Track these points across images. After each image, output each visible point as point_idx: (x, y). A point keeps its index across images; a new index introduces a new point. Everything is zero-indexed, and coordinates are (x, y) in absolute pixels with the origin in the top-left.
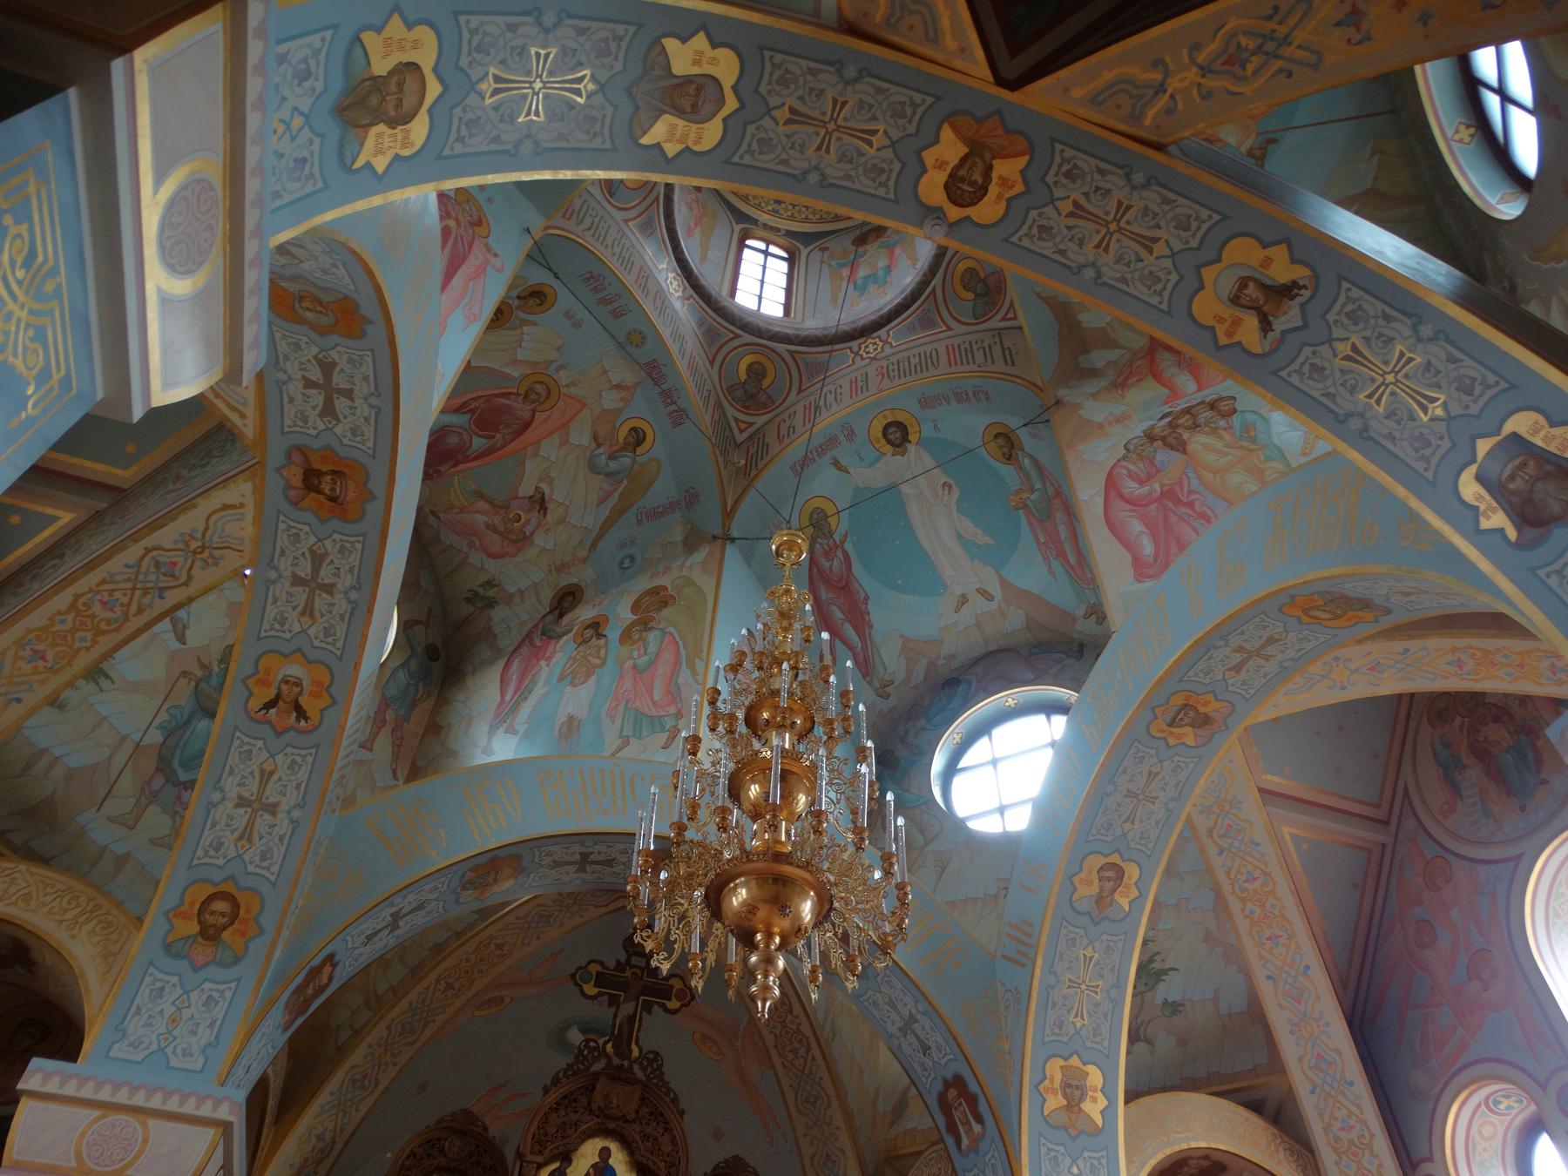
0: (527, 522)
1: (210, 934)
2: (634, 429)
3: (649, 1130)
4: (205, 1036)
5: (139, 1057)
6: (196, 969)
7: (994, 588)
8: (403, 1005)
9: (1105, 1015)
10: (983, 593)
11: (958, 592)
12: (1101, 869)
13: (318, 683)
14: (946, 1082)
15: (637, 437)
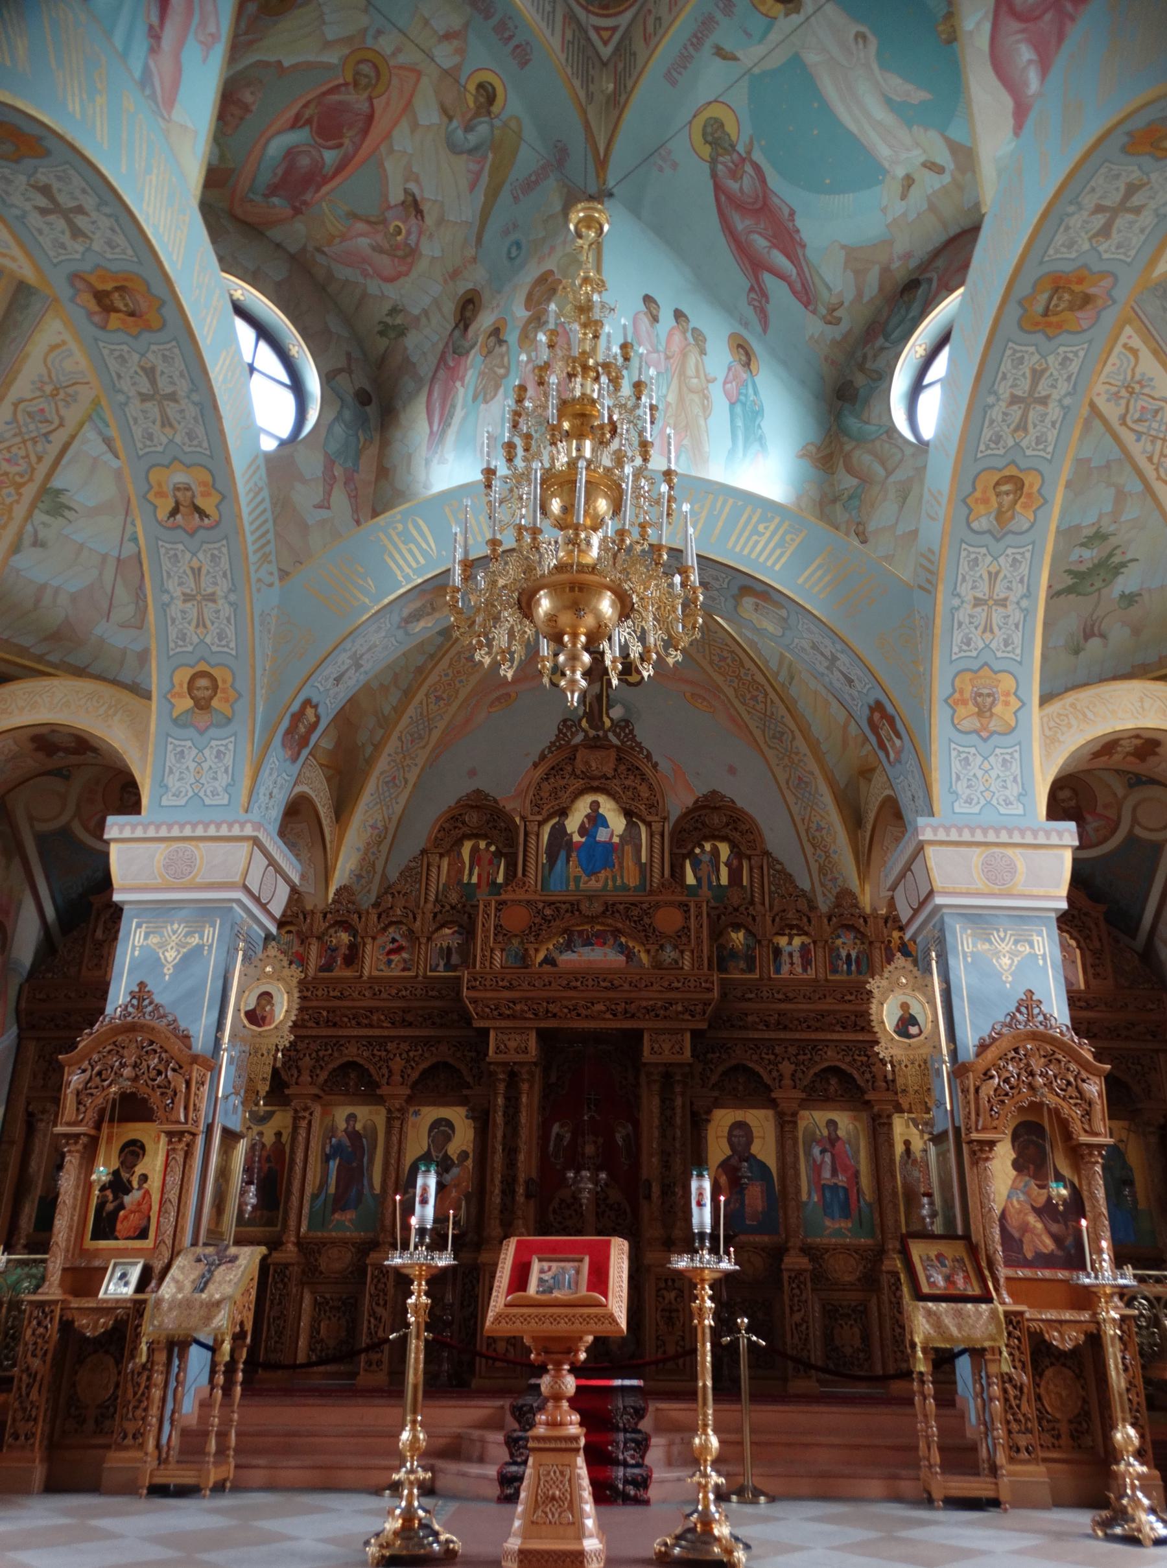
0: (409, 233)
1: (202, 705)
2: (481, 86)
3: (627, 782)
4: (224, 780)
5: (182, 802)
6: (202, 732)
7: (943, 157)
8: (405, 720)
9: (1017, 626)
10: (932, 167)
11: (900, 172)
12: (997, 484)
13: (205, 484)
14: (870, 707)
15: (487, 94)
